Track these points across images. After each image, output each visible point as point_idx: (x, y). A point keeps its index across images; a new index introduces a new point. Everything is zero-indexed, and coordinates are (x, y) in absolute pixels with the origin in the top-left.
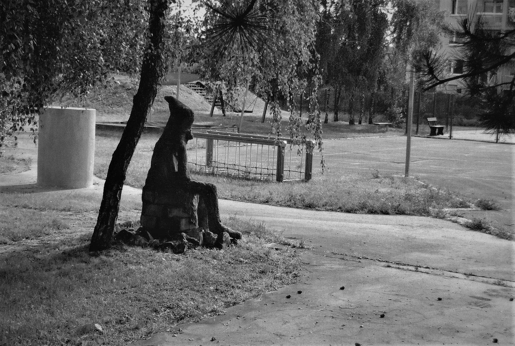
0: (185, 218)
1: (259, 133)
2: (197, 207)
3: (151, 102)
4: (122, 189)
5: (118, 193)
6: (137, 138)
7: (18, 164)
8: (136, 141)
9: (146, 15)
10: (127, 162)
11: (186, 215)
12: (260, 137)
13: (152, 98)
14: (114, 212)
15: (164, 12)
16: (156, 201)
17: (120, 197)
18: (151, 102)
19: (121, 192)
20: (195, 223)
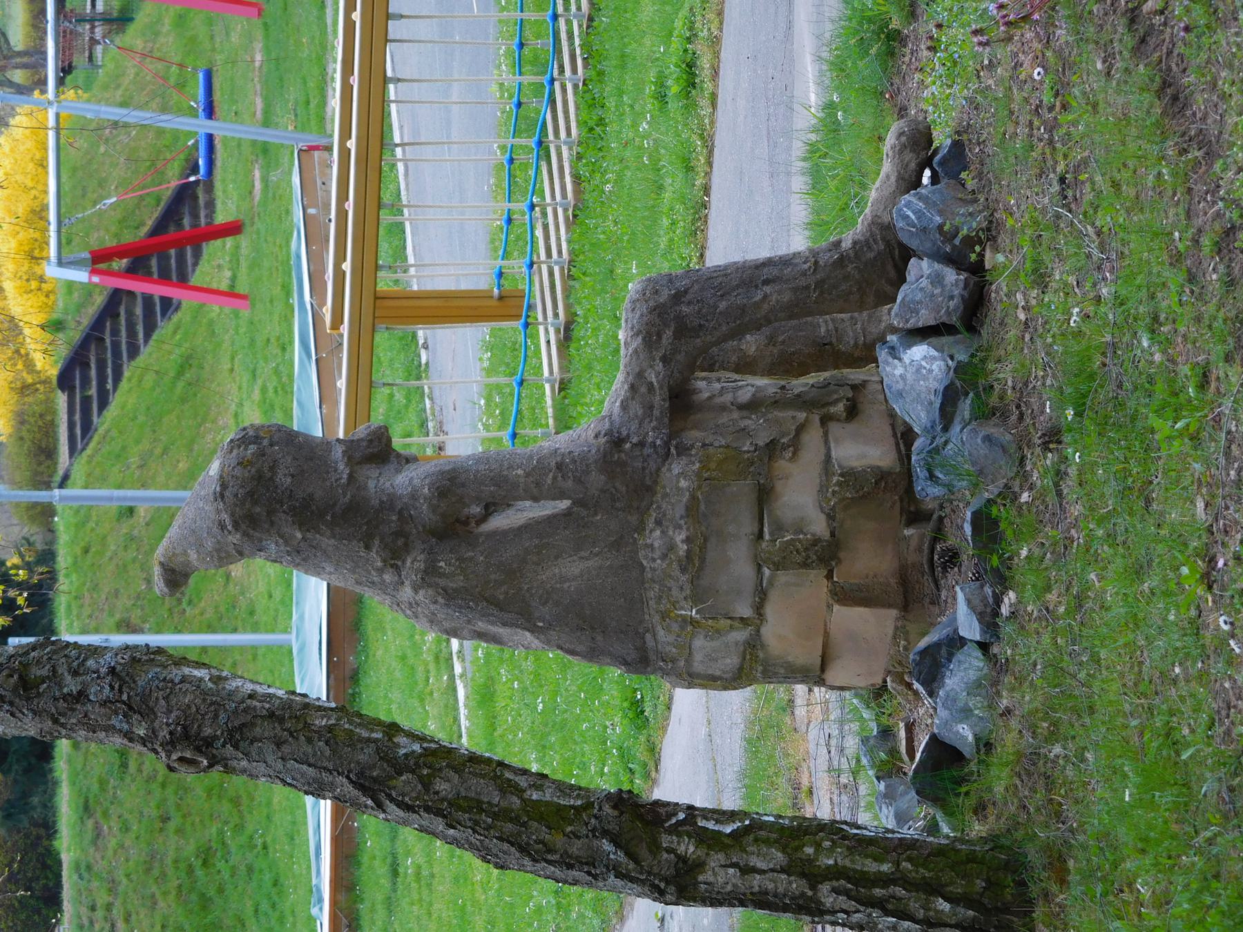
0: (826, 442)
1: (323, 102)
2: (761, 382)
3: (197, 673)
4: (691, 808)
5: (711, 825)
6: (401, 740)
7: (106, 918)
8: (416, 747)
9: (259, 102)
10: (538, 788)
11: (813, 437)
12: (347, 89)
13: (176, 673)
14: (818, 846)
15: (746, 456)
16: (745, 611)
17: (732, 815)
18: (197, 673)
19: (707, 813)
20: (854, 387)
